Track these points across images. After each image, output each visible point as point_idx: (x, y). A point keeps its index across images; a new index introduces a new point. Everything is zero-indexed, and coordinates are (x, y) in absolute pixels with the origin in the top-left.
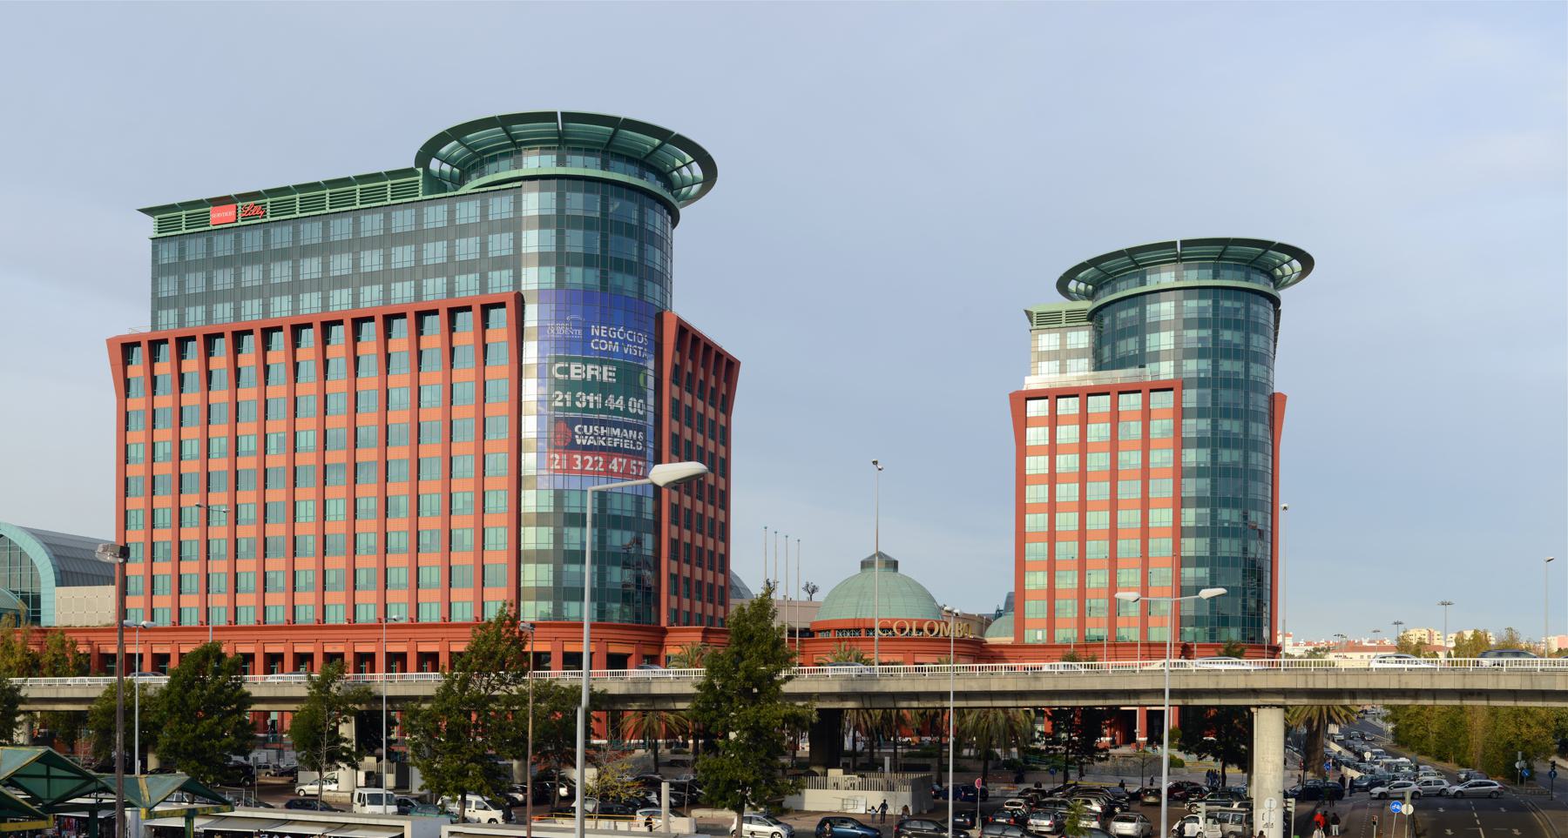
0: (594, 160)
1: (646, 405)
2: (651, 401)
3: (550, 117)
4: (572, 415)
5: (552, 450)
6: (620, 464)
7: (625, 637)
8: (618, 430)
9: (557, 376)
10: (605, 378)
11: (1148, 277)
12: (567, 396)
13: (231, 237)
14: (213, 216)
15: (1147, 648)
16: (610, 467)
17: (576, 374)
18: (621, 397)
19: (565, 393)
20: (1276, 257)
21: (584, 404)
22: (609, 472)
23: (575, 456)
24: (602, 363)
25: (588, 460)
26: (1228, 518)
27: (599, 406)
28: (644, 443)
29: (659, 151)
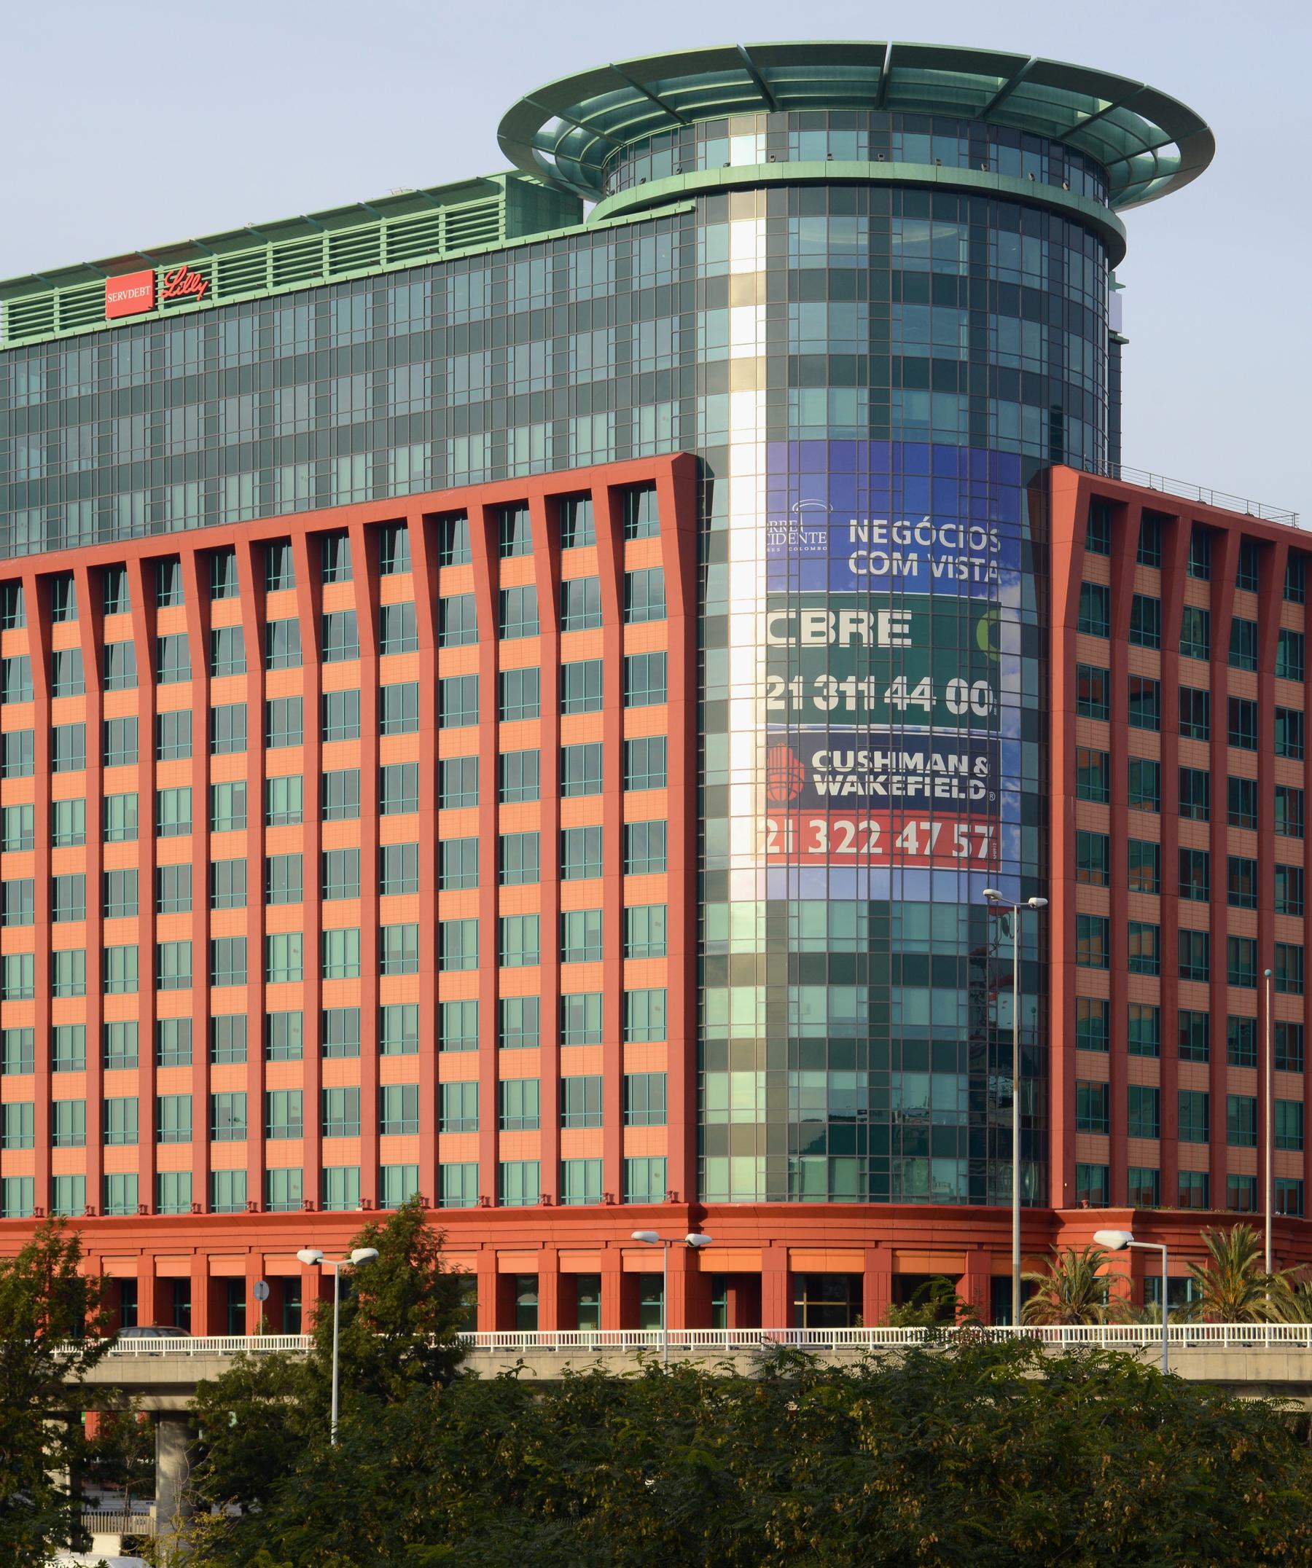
0: (956, 146)
1: (997, 691)
2: (1011, 681)
3: (870, 53)
4: (805, 728)
5: (762, 810)
6: (923, 836)
7: (937, 1236)
8: (919, 757)
9: (773, 640)
10: (884, 639)
12: (793, 687)
13: (142, 344)
14: (110, 298)
16: (898, 843)
17: (814, 634)
18: (926, 680)
19: (789, 680)
21: (834, 703)
22: (896, 856)
23: (813, 823)
24: (874, 605)
25: (843, 832)
27: (870, 704)
28: (992, 782)
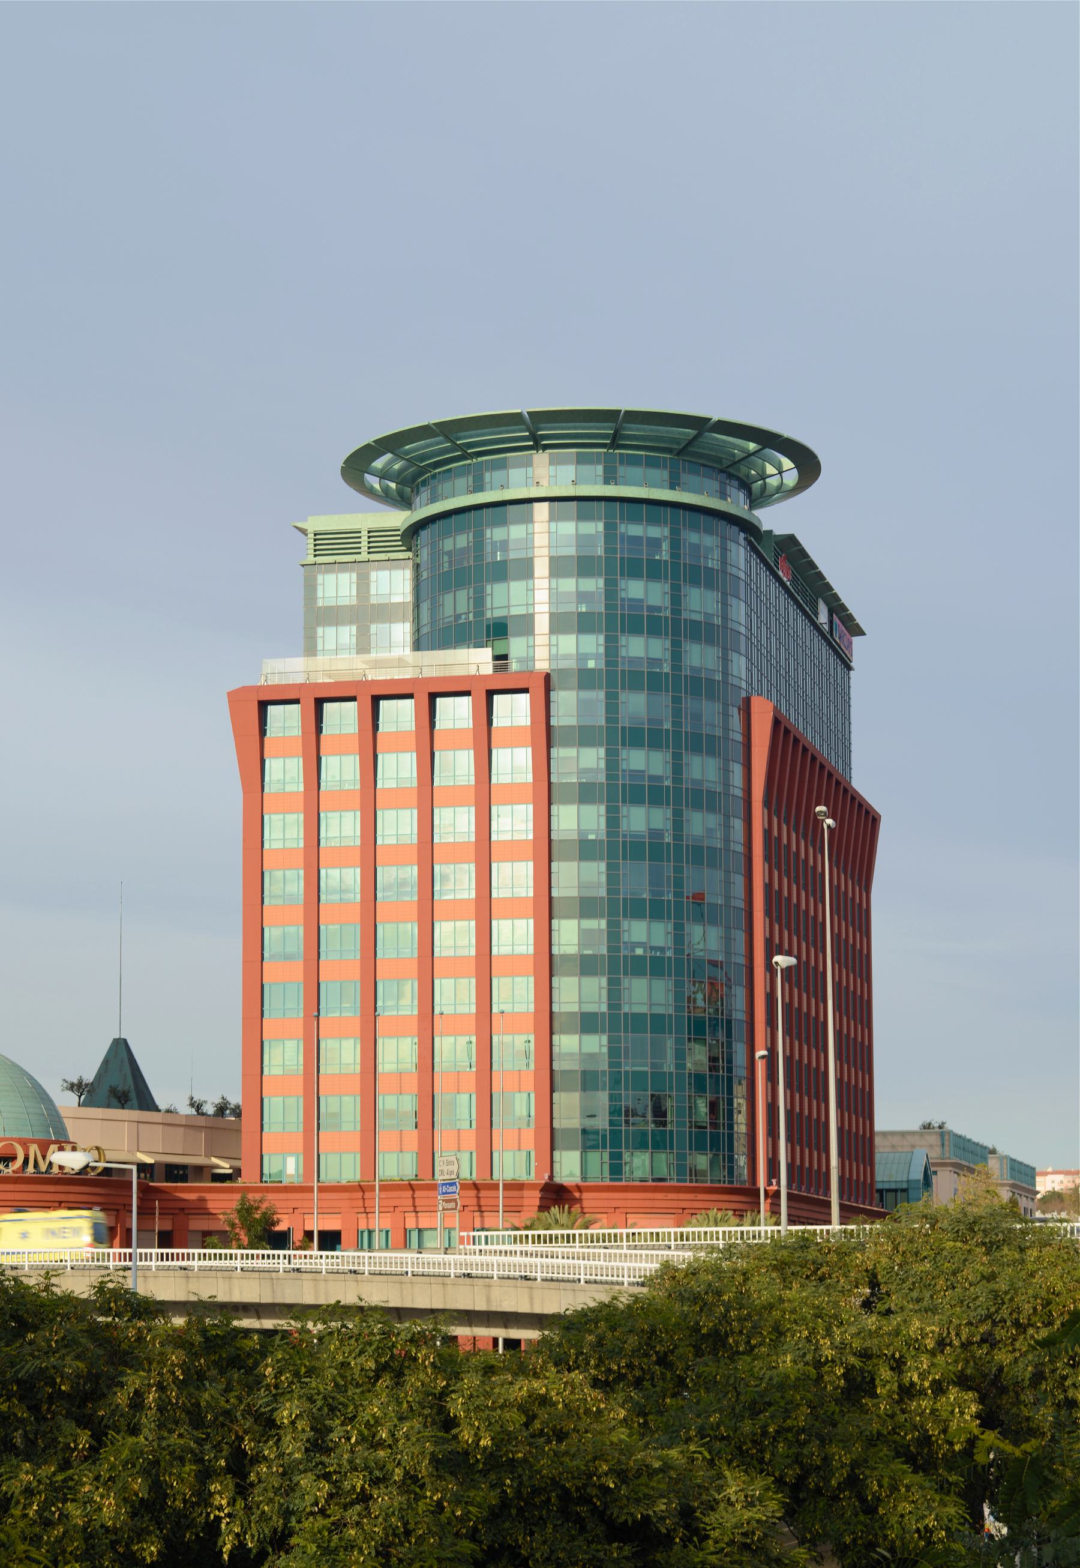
11: (487, 476)
15: (473, 1193)
20: (735, 446)
26: (644, 939)
29: (753, 457)
